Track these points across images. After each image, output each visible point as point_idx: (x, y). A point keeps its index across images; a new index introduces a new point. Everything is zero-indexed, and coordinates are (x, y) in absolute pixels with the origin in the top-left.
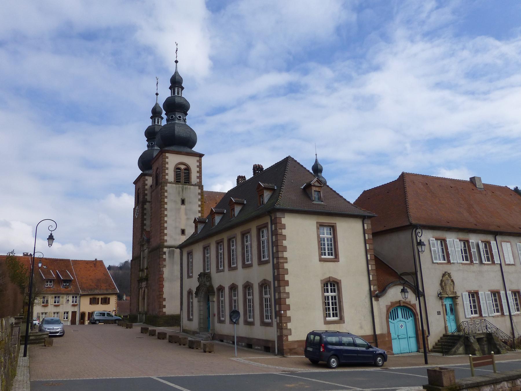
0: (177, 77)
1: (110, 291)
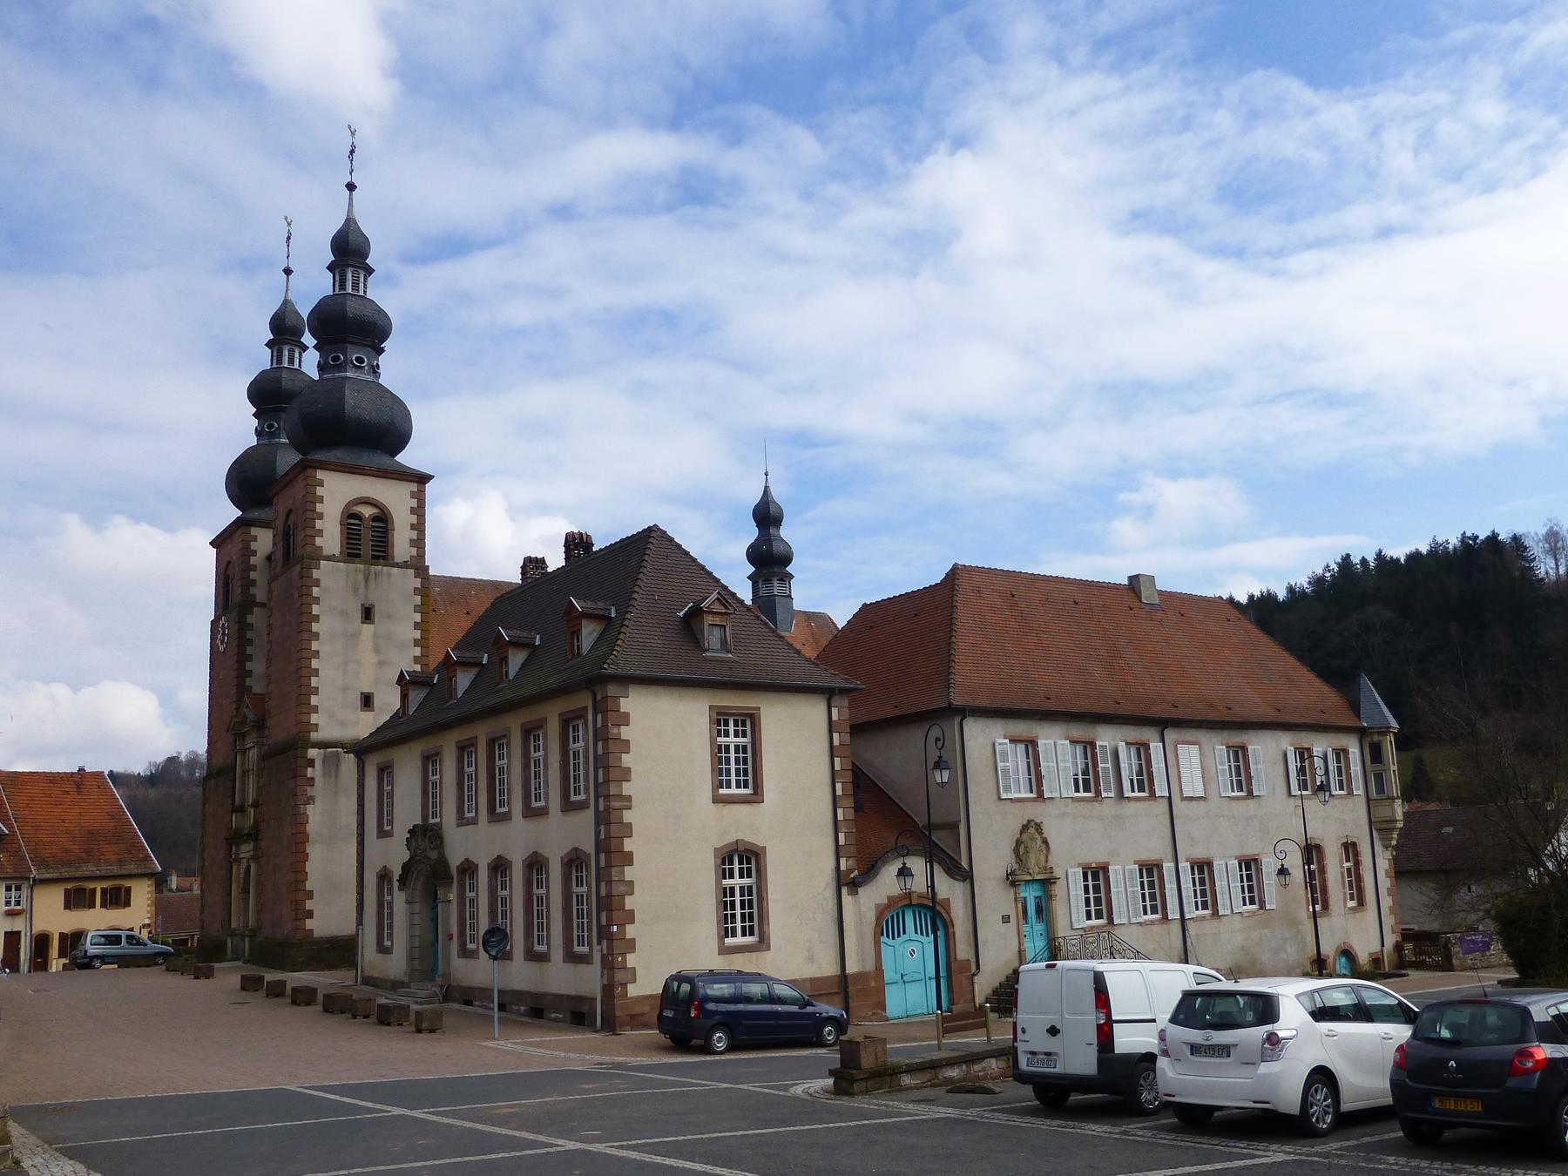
1: (132, 868)
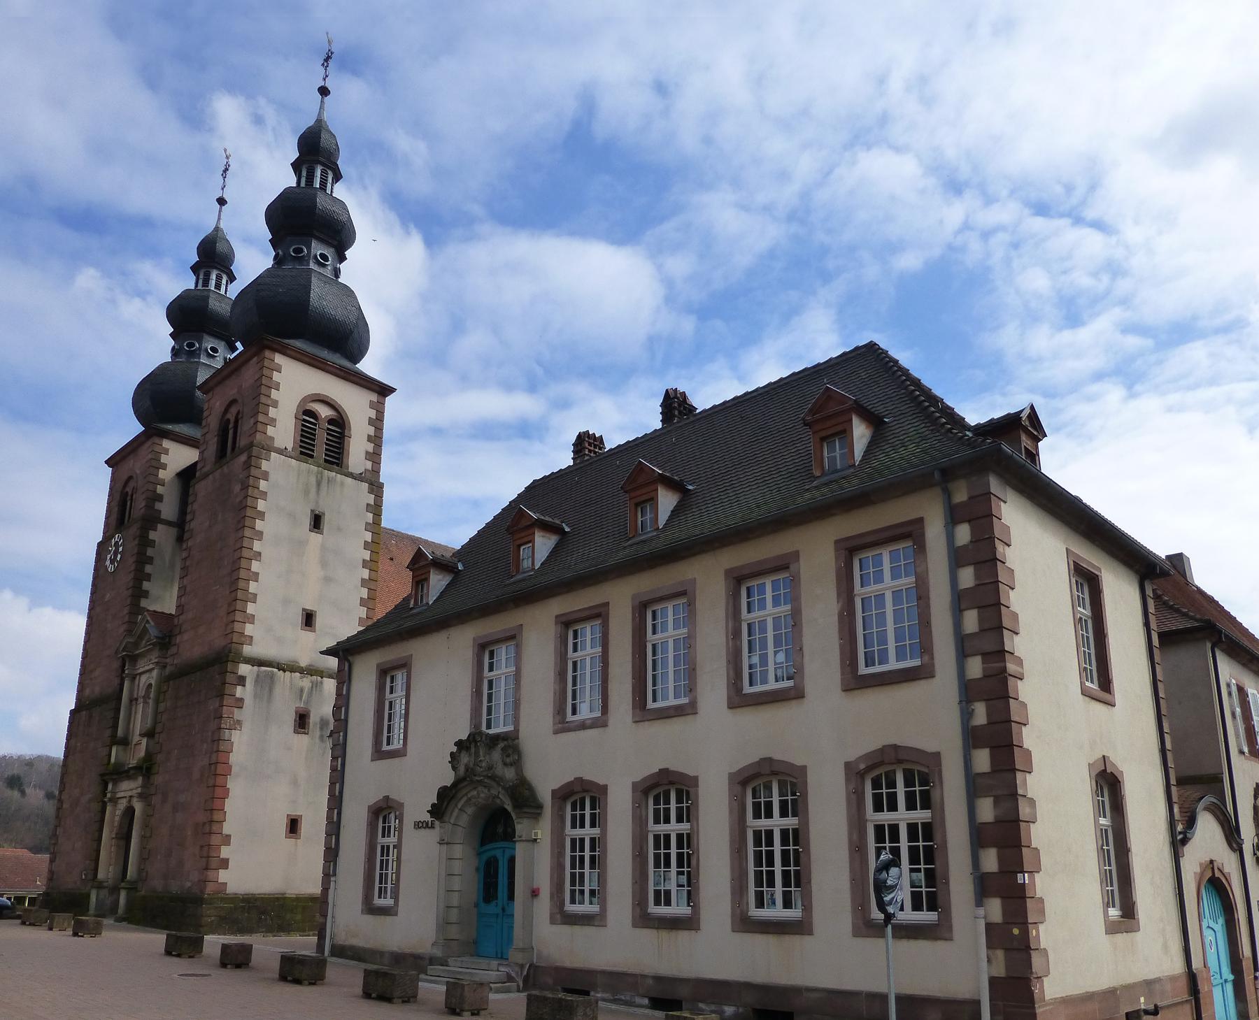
0: (324, 136)
